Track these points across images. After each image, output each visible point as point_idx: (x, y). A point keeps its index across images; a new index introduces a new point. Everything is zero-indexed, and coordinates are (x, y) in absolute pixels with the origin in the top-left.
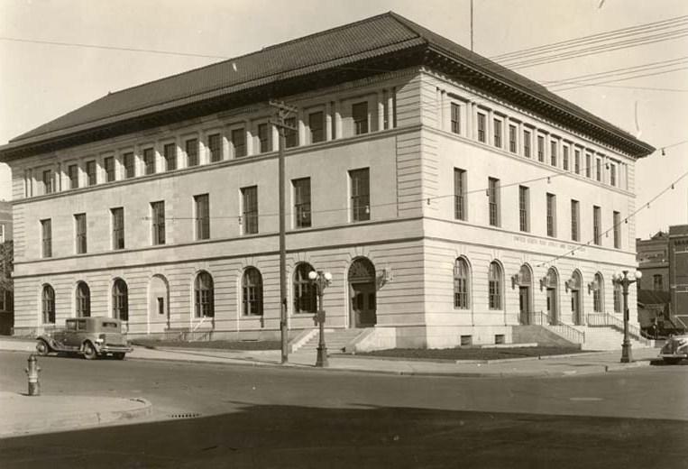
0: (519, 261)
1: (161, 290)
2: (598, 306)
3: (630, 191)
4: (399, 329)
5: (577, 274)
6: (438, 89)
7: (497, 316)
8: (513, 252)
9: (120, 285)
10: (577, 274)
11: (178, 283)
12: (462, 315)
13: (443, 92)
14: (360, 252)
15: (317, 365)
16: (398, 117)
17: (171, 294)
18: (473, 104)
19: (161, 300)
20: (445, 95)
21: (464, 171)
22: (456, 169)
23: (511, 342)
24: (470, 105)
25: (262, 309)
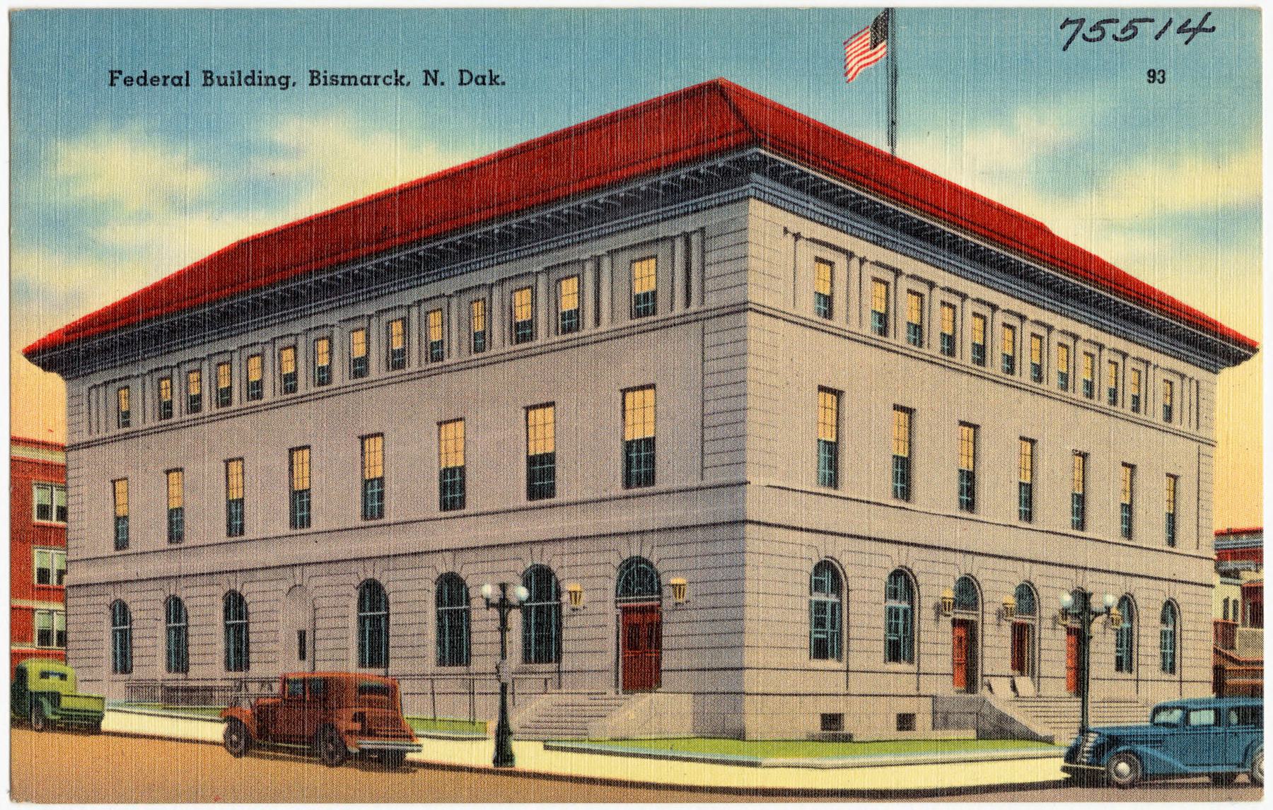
0: (951, 569)
1: (302, 619)
2: (1124, 663)
3: (1203, 433)
4: (700, 698)
5: (1027, 594)
6: (786, 231)
7: (900, 677)
8: (1158, 582)
9: (235, 605)
10: (1027, 594)
11: (333, 601)
12: (827, 675)
13: (797, 236)
14: (633, 549)
15: (1215, 724)
16: (709, 285)
17: (320, 623)
18: (1156, 367)
19: (302, 635)
20: (801, 242)
21: (978, 426)
22: (1169, 475)
23: (687, 728)
24: (855, 263)
25: (469, 654)
